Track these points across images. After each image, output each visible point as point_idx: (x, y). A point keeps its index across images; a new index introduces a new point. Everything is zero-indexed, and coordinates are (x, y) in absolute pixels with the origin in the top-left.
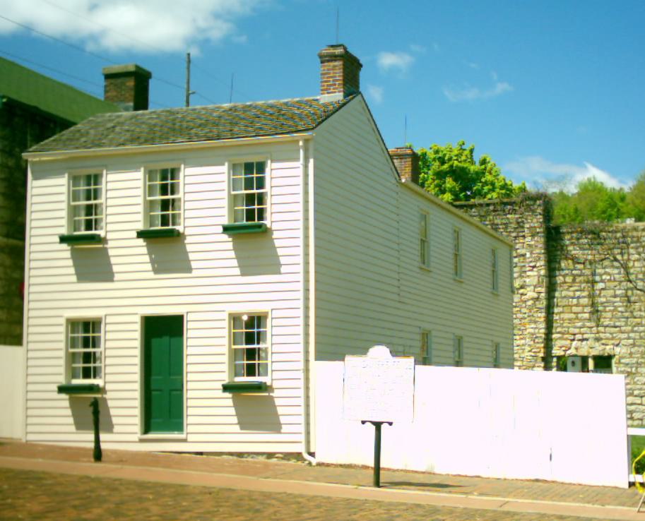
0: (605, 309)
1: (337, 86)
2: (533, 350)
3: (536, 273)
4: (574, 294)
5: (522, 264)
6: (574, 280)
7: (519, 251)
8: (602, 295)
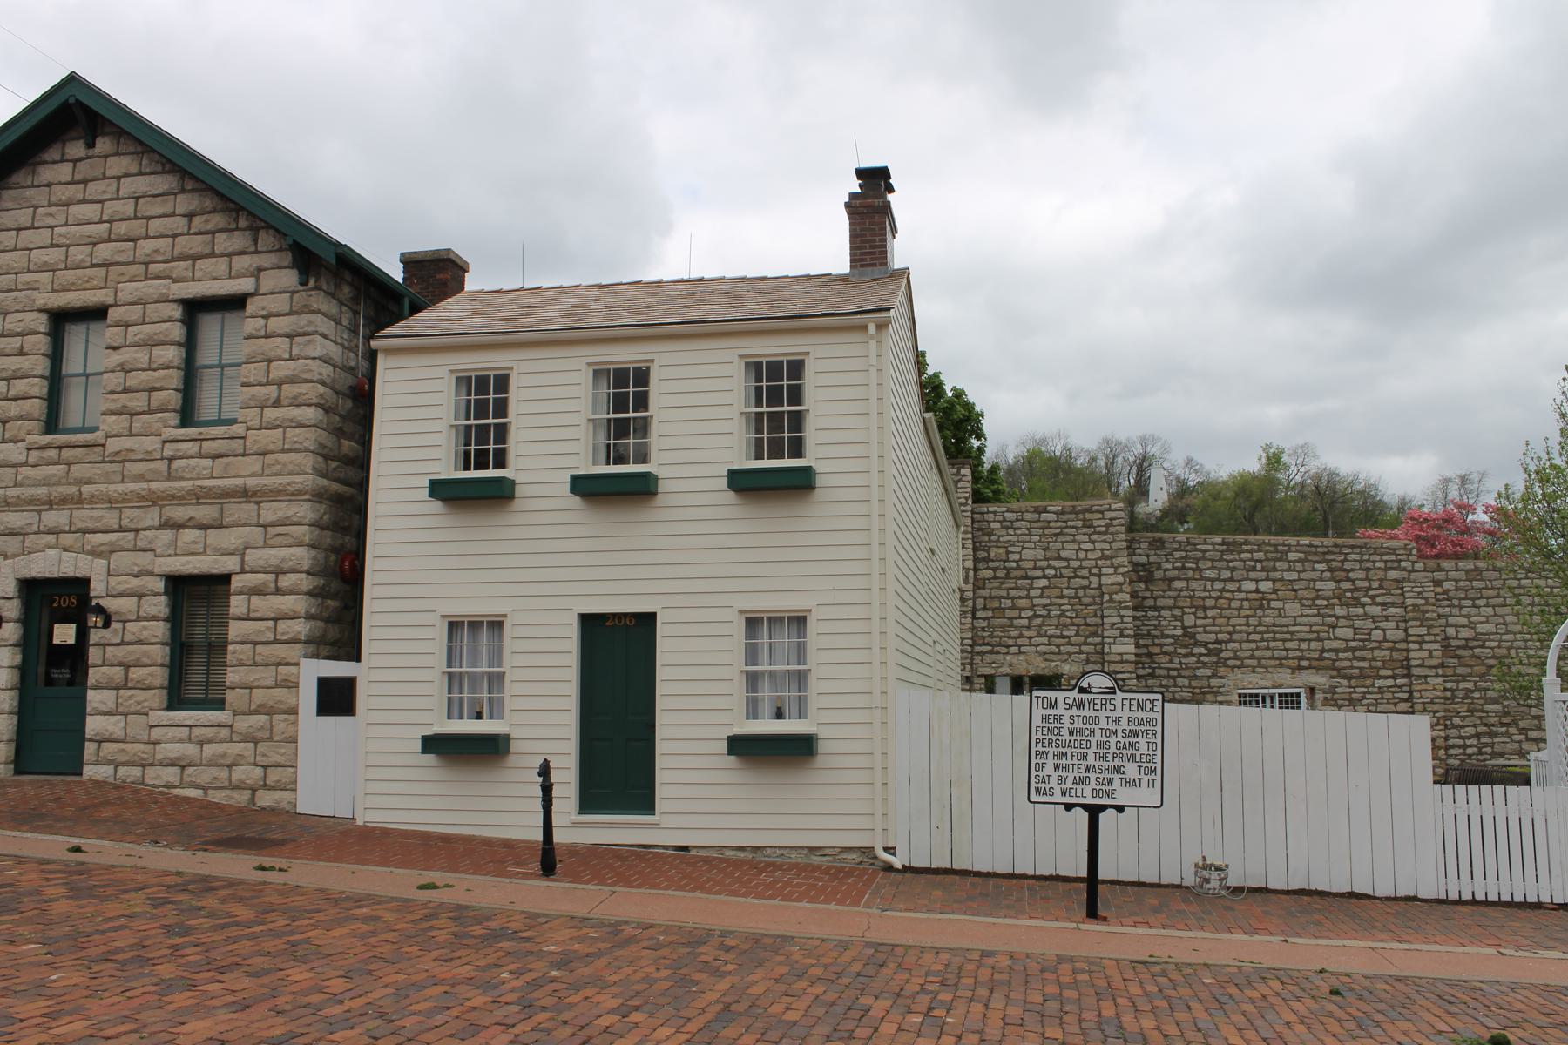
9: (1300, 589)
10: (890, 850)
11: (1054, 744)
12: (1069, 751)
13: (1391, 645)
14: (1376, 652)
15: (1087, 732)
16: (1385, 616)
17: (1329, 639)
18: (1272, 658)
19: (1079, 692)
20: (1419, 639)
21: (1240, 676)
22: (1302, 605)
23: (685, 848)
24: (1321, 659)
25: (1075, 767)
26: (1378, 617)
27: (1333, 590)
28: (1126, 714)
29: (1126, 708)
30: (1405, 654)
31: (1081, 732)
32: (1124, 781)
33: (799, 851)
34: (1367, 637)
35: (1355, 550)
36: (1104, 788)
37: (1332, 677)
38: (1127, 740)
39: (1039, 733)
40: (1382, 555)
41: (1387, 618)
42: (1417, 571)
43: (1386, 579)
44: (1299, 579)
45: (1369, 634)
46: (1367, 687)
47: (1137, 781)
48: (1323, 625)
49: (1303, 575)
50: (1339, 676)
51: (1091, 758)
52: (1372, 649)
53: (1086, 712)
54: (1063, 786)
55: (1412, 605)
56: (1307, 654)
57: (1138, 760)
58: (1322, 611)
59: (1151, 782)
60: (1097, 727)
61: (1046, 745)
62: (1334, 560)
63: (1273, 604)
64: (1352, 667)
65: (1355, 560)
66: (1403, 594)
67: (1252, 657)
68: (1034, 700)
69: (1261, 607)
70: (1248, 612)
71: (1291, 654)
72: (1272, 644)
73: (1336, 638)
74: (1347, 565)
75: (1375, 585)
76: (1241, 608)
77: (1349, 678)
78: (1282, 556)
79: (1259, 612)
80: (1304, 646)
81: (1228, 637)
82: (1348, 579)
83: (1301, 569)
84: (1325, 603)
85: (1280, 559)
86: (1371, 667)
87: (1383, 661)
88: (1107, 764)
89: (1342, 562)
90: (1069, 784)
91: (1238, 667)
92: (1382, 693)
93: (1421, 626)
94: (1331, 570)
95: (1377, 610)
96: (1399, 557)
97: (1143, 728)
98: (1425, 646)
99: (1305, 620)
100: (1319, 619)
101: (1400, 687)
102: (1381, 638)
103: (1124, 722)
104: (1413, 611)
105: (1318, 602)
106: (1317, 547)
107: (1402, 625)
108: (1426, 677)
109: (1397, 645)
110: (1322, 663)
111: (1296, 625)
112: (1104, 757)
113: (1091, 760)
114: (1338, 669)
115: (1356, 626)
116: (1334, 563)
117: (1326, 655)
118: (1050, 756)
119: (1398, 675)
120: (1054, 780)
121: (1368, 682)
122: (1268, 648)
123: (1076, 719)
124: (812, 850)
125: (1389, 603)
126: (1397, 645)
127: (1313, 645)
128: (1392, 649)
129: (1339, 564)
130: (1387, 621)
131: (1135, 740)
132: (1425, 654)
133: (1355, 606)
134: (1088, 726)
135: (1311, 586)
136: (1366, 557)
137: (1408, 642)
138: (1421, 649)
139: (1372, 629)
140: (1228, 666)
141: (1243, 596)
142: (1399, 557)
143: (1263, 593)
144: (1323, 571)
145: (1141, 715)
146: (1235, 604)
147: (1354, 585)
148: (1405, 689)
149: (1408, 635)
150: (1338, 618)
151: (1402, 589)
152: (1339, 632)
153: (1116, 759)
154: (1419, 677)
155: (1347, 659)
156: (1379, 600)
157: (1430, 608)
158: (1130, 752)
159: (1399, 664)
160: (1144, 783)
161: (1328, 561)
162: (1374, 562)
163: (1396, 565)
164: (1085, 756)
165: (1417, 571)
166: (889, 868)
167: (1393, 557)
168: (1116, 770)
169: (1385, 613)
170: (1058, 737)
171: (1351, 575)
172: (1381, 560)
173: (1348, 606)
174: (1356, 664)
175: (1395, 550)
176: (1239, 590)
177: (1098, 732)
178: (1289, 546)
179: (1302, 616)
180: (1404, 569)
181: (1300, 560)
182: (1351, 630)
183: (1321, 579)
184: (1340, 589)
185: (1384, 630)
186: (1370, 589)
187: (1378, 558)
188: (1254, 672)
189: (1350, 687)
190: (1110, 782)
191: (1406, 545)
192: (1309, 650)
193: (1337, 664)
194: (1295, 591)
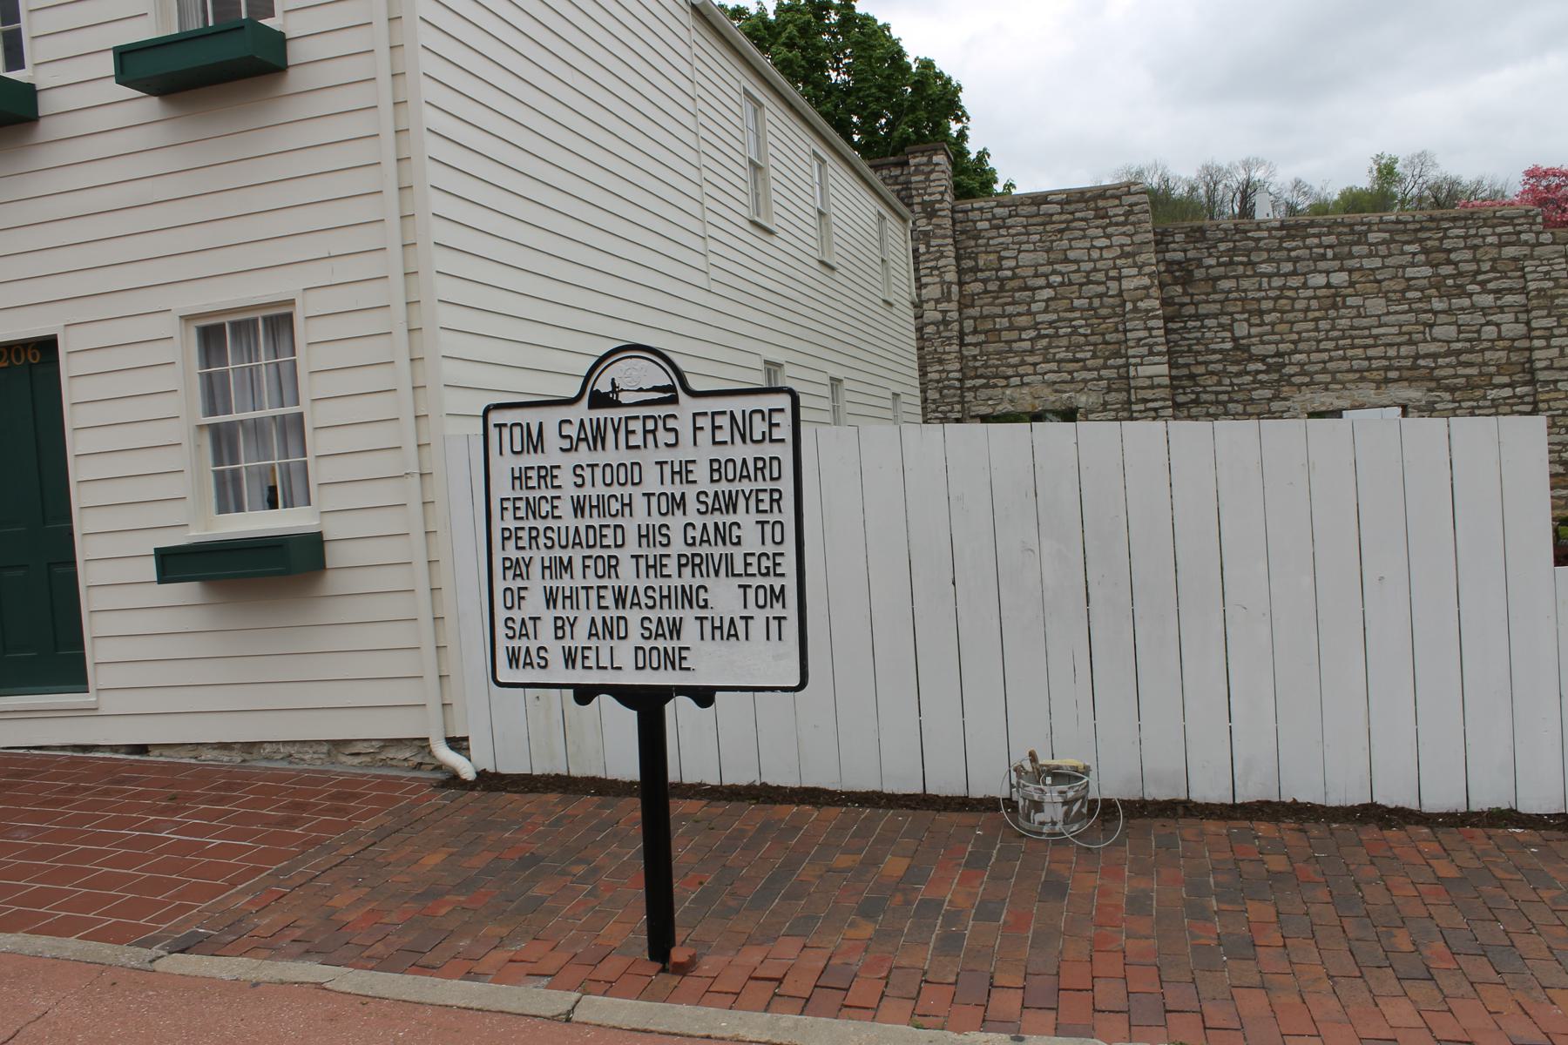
4: (1004, 311)
6: (1002, 288)
9: (1385, 279)
10: (458, 744)
11: (542, 540)
12: (577, 554)
13: (1507, 343)
14: (1488, 355)
15: (615, 506)
16: (1500, 307)
17: (1425, 341)
18: (1350, 370)
19: (592, 406)
20: (1547, 333)
21: (1309, 396)
22: (1388, 300)
23: (142, 749)
24: (1415, 367)
25: (593, 594)
26: (1490, 308)
27: (1430, 277)
28: (704, 452)
29: (704, 437)
30: (1527, 354)
31: (601, 506)
32: (707, 625)
33: (316, 748)
34: (1476, 335)
35: (1459, 224)
36: (660, 644)
37: (1430, 390)
38: (710, 520)
39: (509, 515)
40: (1494, 227)
41: (1501, 309)
42: (1543, 244)
43: (1500, 258)
44: (1384, 267)
45: (1478, 332)
46: (1477, 400)
47: (740, 625)
48: (1417, 323)
49: (1389, 261)
50: (1439, 388)
51: (627, 569)
52: (1482, 351)
53: (611, 455)
54: (567, 642)
55: (1539, 290)
56: (1396, 363)
57: (739, 569)
58: (1414, 306)
59: (774, 625)
60: (637, 492)
61: (524, 543)
62: (1429, 238)
63: (1349, 301)
64: (1456, 376)
65: (1458, 237)
66: (1523, 276)
67: (1324, 371)
68: (494, 433)
69: (1334, 306)
70: (1317, 314)
71: (1375, 364)
72: (1350, 353)
73: (1434, 340)
74: (1447, 244)
75: (1486, 266)
76: (1307, 310)
77: (1452, 389)
78: (1359, 238)
79: (1332, 313)
80: (1392, 352)
81: (1292, 346)
82: (1449, 262)
83: (1386, 253)
84: (1418, 294)
85: (1358, 243)
86: (1481, 374)
87: (1498, 366)
88: (665, 583)
89: (1441, 240)
90: (581, 638)
91: (1307, 385)
92: (1496, 407)
93: (1549, 315)
94: (1425, 251)
95: (1488, 300)
96: (1518, 228)
97: (746, 486)
98: (1554, 342)
99: (1391, 318)
100: (1411, 317)
101: (1521, 397)
102: (1495, 336)
103: (701, 473)
104: (1537, 297)
105: (1409, 295)
106: (1406, 223)
107: (1523, 317)
108: (1555, 382)
109: (1516, 344)
110: (1416, 373)
111: (1380, 326)
112: (657, 566)
113: (627, 575)
114: (1438, 380)
115: (1460, 322)
116: (1429, 242)
117: (1421, 362)
118: (536, 569)
119: (1518, 382)
120: (546, 630)
121: (1478, 393)
122: (1344, 358)
123: (587, 473)
124: (337, 744)
125: (1504, 289)
126: (1516, 344)
127: (1404, 350)
128: (1510, 349)
129: (1437, 243)
130: (1503, 312)
131: (730, 518)
132: (1555, 352)
133: (1459, 296)
134: (616, 490)
135: (1400, 274)
136: (1473, 232)
137: (1531, 339)
138: (1548, 347)
139: (1482, 325)
140: (1293, 385)
141: (1310, 293)
142: (1518, 228)
143: (1336, 288)
144: (1414, 254)
145: (742, 452)
146: (1300, 305)
147: (1457, 268)
148: (1527, 399)
149: (1531, 329)
150: (1435, 313)
151: (1523, 269)
152: (1437, 331)
153: (687, 571)
154: (1546, 383)
155: (1448, 365)
156: (1490, 286)
157: (1561, 292)
158: (718, 550)
159: (1519, 368)
160: (757, 627)
161: (1421, 241)
162: (1484, 237)
163: (1514, 238)
164: (612, 566)
165: (1543, 244)
166: (453, 780)
167: (1510, 229)
168: (688, 597)
169: (1499, 303)
170: (550, 522)
171: (1453, 256)
172: (1494, 234)
173: (1450, 297)
174: (1461, 371)
175: (1513, 218)
176: (1305, 286)
177: (640, 504)
178: (1369, 224)
179: (1388, 313)
180: (1526, 243)
181: (1384, 242)
182: (1454, 328)
183: (1413, 265)
184: (1439, 275)
185: (1498, 325)
186: (1478, 272)
187: (1489, 231)
188: (1327, 389)
189: (1454, 401)
190: (676, 629)
191: (1527, 211)
192: (1398, 357)
193: (1436, 373)
194: (1379, 282)
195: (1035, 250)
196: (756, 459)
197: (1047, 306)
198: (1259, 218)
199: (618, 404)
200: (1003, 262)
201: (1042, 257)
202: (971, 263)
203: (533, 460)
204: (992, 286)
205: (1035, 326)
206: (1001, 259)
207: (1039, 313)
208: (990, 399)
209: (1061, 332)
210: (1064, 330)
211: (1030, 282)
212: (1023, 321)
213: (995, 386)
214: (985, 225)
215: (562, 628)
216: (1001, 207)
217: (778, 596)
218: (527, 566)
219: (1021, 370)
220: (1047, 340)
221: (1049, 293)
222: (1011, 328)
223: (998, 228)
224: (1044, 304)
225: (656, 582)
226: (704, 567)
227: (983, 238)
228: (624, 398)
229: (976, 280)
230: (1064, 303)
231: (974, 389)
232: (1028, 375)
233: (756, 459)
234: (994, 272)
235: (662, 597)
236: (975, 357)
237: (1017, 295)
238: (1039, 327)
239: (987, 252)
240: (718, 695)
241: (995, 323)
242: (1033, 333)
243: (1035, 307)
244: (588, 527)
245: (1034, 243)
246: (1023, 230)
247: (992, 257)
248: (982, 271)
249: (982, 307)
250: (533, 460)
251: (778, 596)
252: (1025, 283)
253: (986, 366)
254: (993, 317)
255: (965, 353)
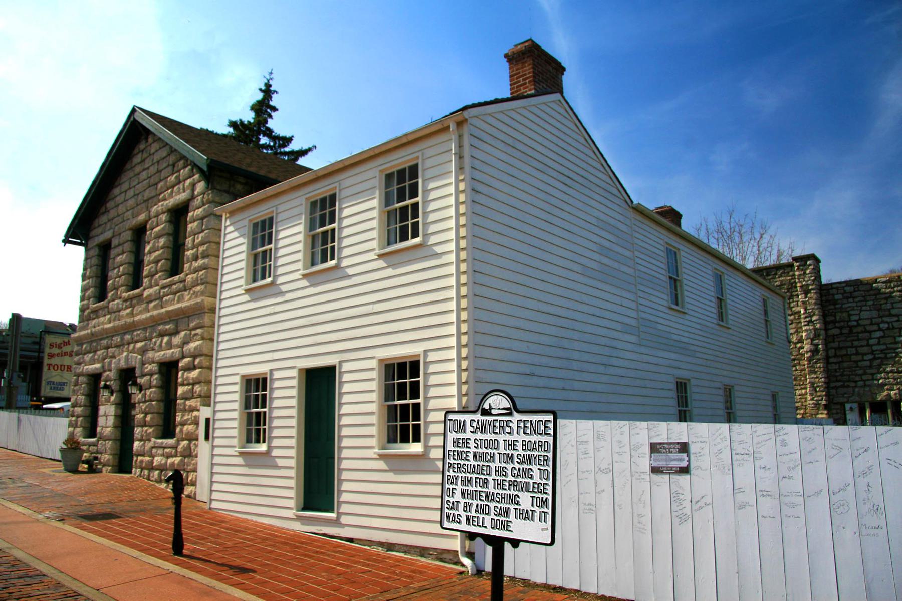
0: (886, 356)
1: (527, 85)
2: (815, 399)
3: (811, 327)
4: (852, 344)
5: (798, 321)
6: (851, 331)
7: (793, 309)
8: (881, 342)
36: (501, 518)
88: (504, 492)
97: (536, 453)
112: (500, 485)
113: (491, 489)
134: (489, 451)
145: (535, 438)
160: (537, 515)
190: (506, 512)
195: (871, 310)
196: (539, 441)
197: (879, 341)
198: (375, 408)
199: (491, 414)
200: (851, 317)
201: (875, 313)
202: (832, 318)
203: (461, 435)
204: (845, 331)
205: (872, 352)
206: (850, 315)
207: (874, 345)
208: (845, 393)
209: (889, 355)
210: (891, 354)
211: (868, 328)
212: (865, 349)
213: (848, 386)
214: (840, 297)
215: (466, 507)
216: (849, 286)
217: (544, 502)
218: (456, 479)
219: (864, 377)
220: (880, 360)
221: (878, 334)
222: (857, 354)
223: (847, 298)
224: (877, 340)
225: (500, 492)
226: (518, 487)
227: (839, 304)
228: (493, 412)
229: (836, 327)
230: (889, 340)
231: (836, 388)
232: (868, 380)
233: (539, 441)
234: (846, 323)
235: (502, 498)
236: (836, 370)
237: (860, 335)
238: (875, 352)
239: (842, 312)
240: (521, 544)
241: (847, 351)
242: (871, 357)
243: (872, 342)
244: (478, 465)
245: (870, 306)
246: (862, 299)
247: (845, 314)
248: (839, 322)
249: (839, 342)
250: (461, 435)
251: (544, 502)
252: (865, 328)
253: (842, 375)
254: (847, 347)
255: (830, 368)
